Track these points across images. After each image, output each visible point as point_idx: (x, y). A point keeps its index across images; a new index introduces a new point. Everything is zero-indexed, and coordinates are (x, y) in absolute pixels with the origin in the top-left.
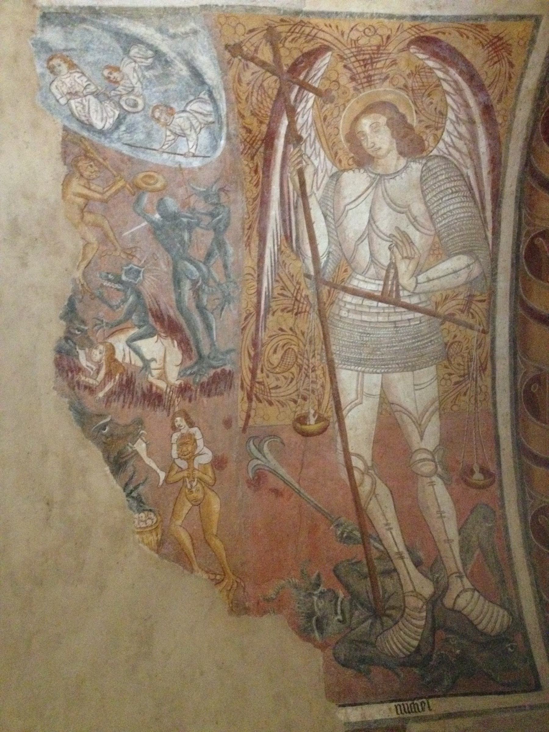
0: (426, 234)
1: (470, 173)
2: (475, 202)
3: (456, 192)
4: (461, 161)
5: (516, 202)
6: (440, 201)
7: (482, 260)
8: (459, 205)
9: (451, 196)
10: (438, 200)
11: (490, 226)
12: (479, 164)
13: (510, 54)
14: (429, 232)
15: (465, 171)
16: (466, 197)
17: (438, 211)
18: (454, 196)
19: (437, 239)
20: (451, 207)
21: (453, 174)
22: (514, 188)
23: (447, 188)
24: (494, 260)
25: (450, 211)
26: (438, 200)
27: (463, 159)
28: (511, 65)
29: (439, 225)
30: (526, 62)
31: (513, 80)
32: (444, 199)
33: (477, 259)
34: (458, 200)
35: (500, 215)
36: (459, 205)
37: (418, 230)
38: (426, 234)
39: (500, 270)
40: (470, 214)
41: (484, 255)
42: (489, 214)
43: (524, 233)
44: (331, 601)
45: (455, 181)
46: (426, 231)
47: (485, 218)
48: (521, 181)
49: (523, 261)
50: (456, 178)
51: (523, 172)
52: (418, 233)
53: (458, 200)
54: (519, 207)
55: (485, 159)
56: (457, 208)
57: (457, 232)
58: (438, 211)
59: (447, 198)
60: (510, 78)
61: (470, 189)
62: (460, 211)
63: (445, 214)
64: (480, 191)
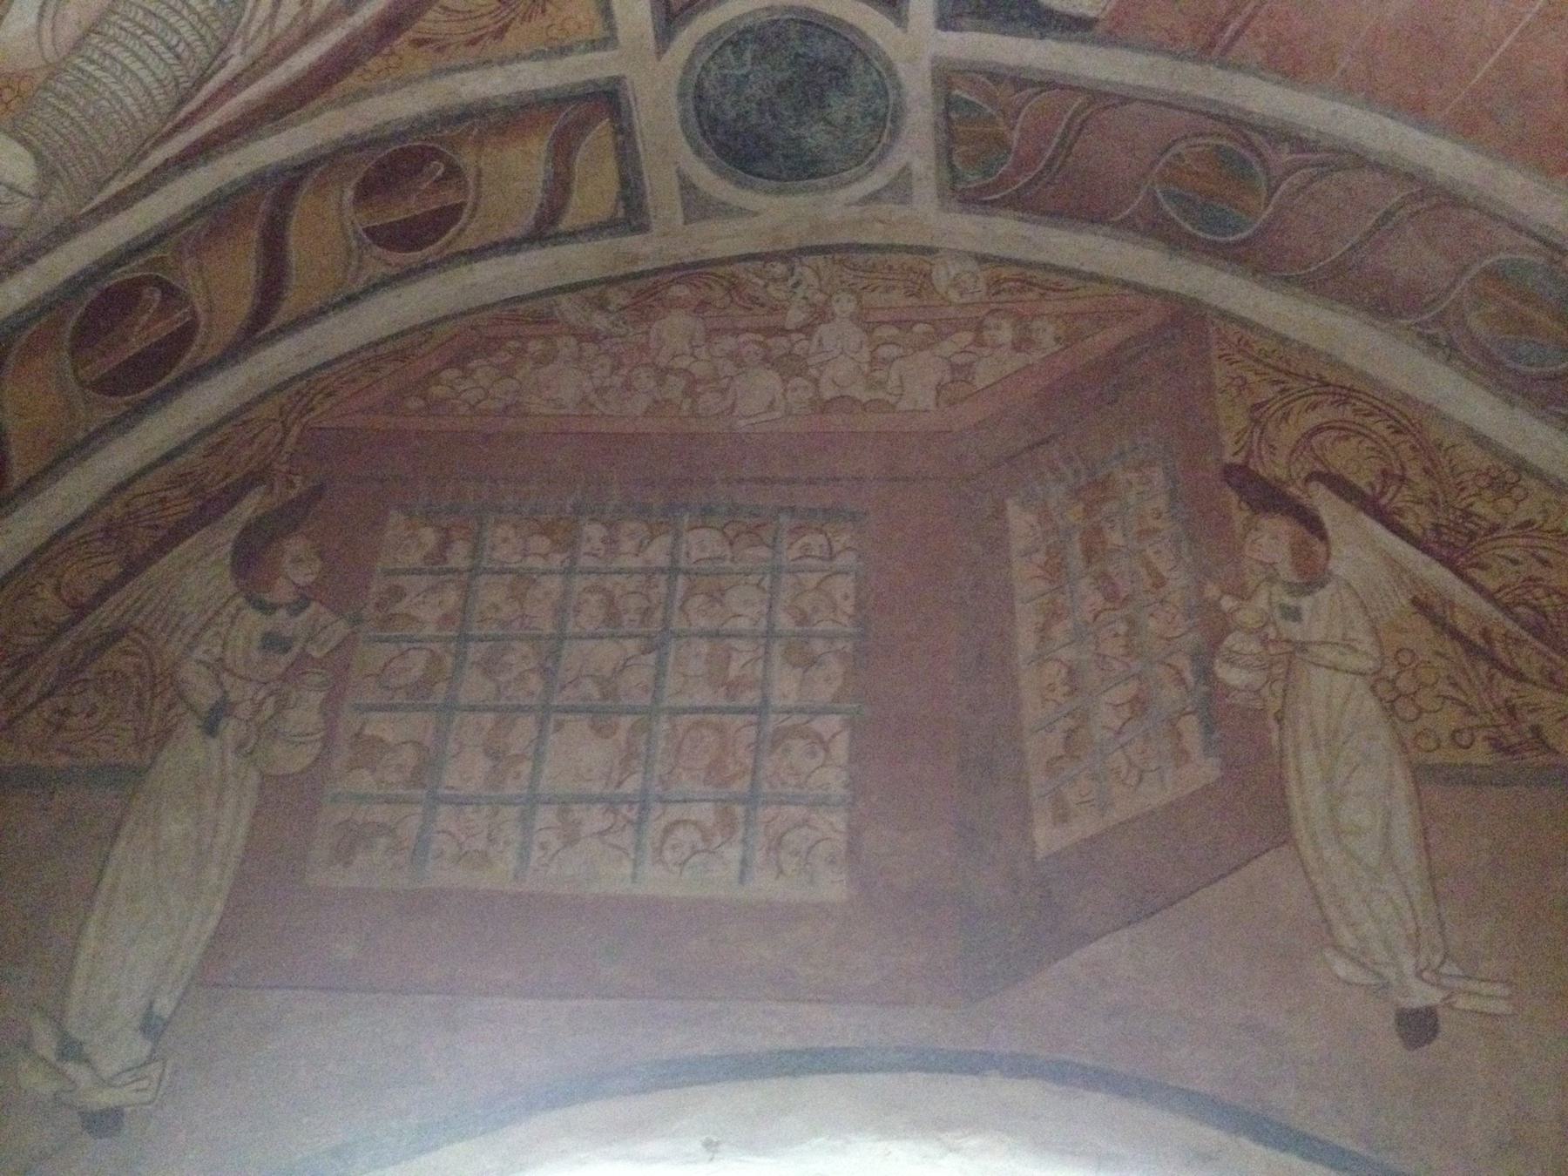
0: (40, 43)
1: (236, 63)
2: (174, 112)
3: (178, 57)
4: (253, 28)
5: (211, 195)
6: (139, 32)
7: (46, 208)
8: (148, 80)
9: (162, 49)
10: (141, 26)
11: (135, 176)
12: (258, 76)
13: (523, 19)
14: (48, 46)
15: (236, 47)
16: (177, 85)
17: (114, 39)
18: (168, 56)
19: (40, 77)
20: (136, 66)
21: (215, 26)
22: (239, 173)
23: (176, 31)
24: (66, 231)
25: (125, 68)
26: (141, 26)
27: (259, 31)
28: (500, 33)
29: (78, 61)
30: (519, 57)
31: (474, 50)
32: (147, 38)
33: (42, 197)
34: (161, 72)
35: (164, 182)
36: (148, 80)
37: (41, 16)
38: (40, 43)
39: (44, 262)
40: (139, 116)
41: (59, 203)
42: (157, 157)
43: (155, 253)
44: (1485, 634)
45: (202, 38)
46: (47, 35)
47: (145, 155)
48: (259, 179)
49: (92, 293)
50: (209, 38)
51: (280, 170)
52: (33, 20)
53: (161, 72)
54: (202, 209)
55: (278, 77)
56: (140, 80)
57: (83, 111)
58: (114, 39)
59: (155, 43)
60: (473, 42)
61: (200, 82)
62: (138, 90)
63: (114, 59)
64: (200, 109)
